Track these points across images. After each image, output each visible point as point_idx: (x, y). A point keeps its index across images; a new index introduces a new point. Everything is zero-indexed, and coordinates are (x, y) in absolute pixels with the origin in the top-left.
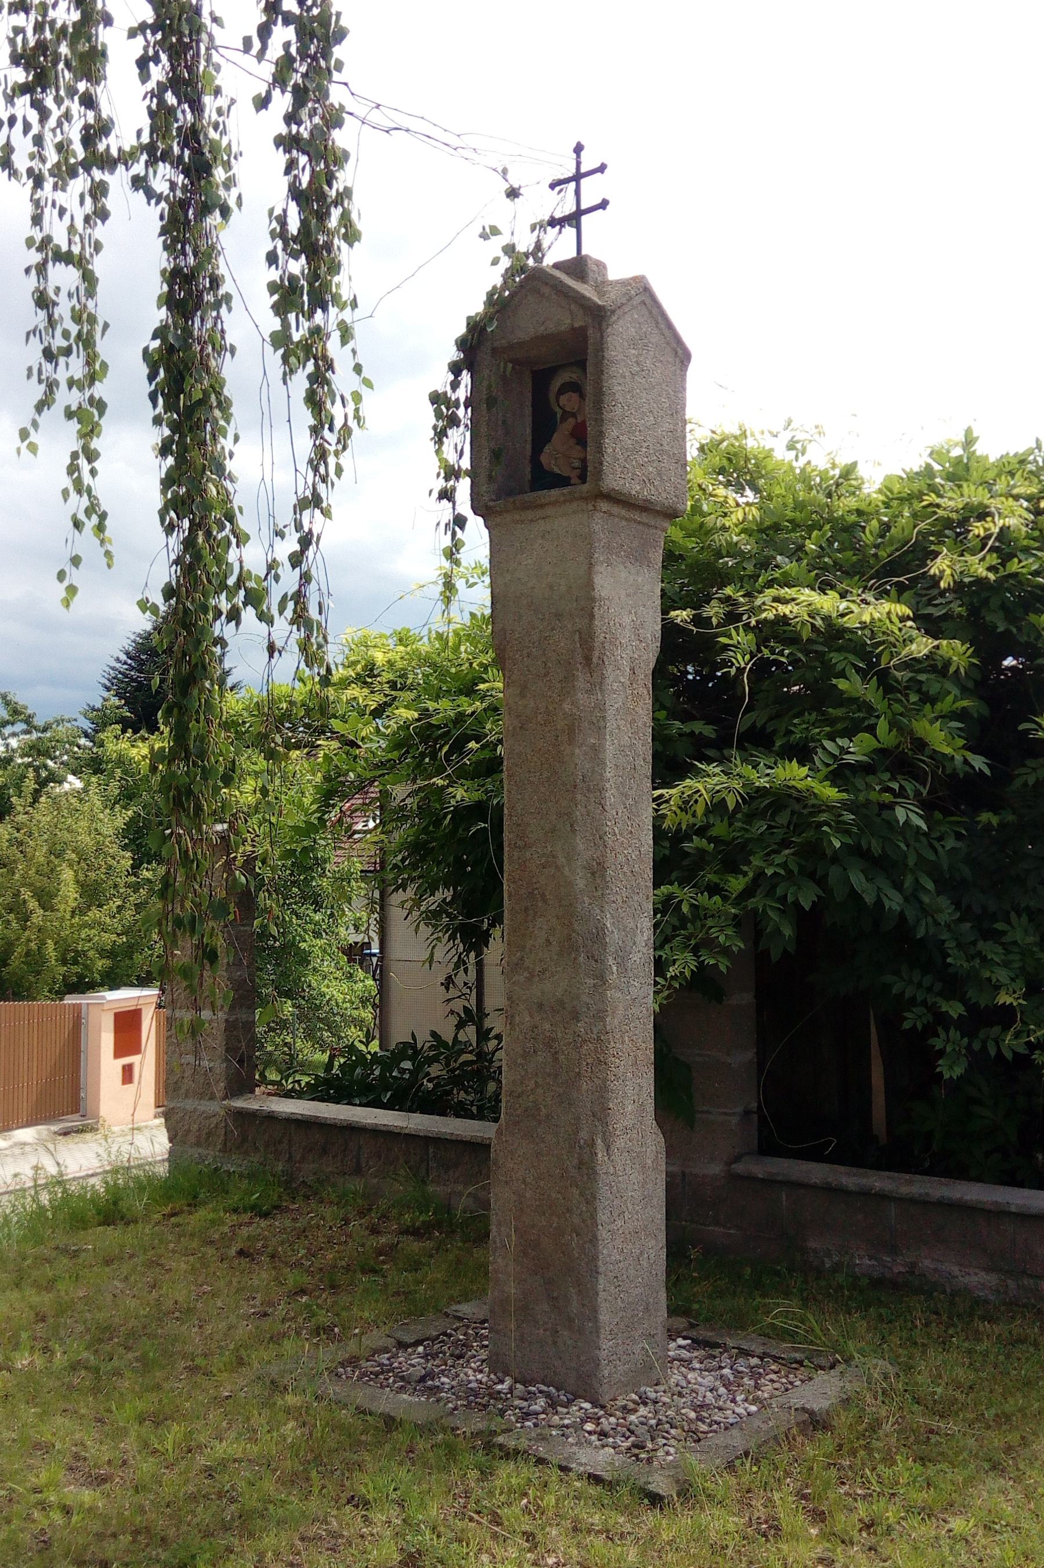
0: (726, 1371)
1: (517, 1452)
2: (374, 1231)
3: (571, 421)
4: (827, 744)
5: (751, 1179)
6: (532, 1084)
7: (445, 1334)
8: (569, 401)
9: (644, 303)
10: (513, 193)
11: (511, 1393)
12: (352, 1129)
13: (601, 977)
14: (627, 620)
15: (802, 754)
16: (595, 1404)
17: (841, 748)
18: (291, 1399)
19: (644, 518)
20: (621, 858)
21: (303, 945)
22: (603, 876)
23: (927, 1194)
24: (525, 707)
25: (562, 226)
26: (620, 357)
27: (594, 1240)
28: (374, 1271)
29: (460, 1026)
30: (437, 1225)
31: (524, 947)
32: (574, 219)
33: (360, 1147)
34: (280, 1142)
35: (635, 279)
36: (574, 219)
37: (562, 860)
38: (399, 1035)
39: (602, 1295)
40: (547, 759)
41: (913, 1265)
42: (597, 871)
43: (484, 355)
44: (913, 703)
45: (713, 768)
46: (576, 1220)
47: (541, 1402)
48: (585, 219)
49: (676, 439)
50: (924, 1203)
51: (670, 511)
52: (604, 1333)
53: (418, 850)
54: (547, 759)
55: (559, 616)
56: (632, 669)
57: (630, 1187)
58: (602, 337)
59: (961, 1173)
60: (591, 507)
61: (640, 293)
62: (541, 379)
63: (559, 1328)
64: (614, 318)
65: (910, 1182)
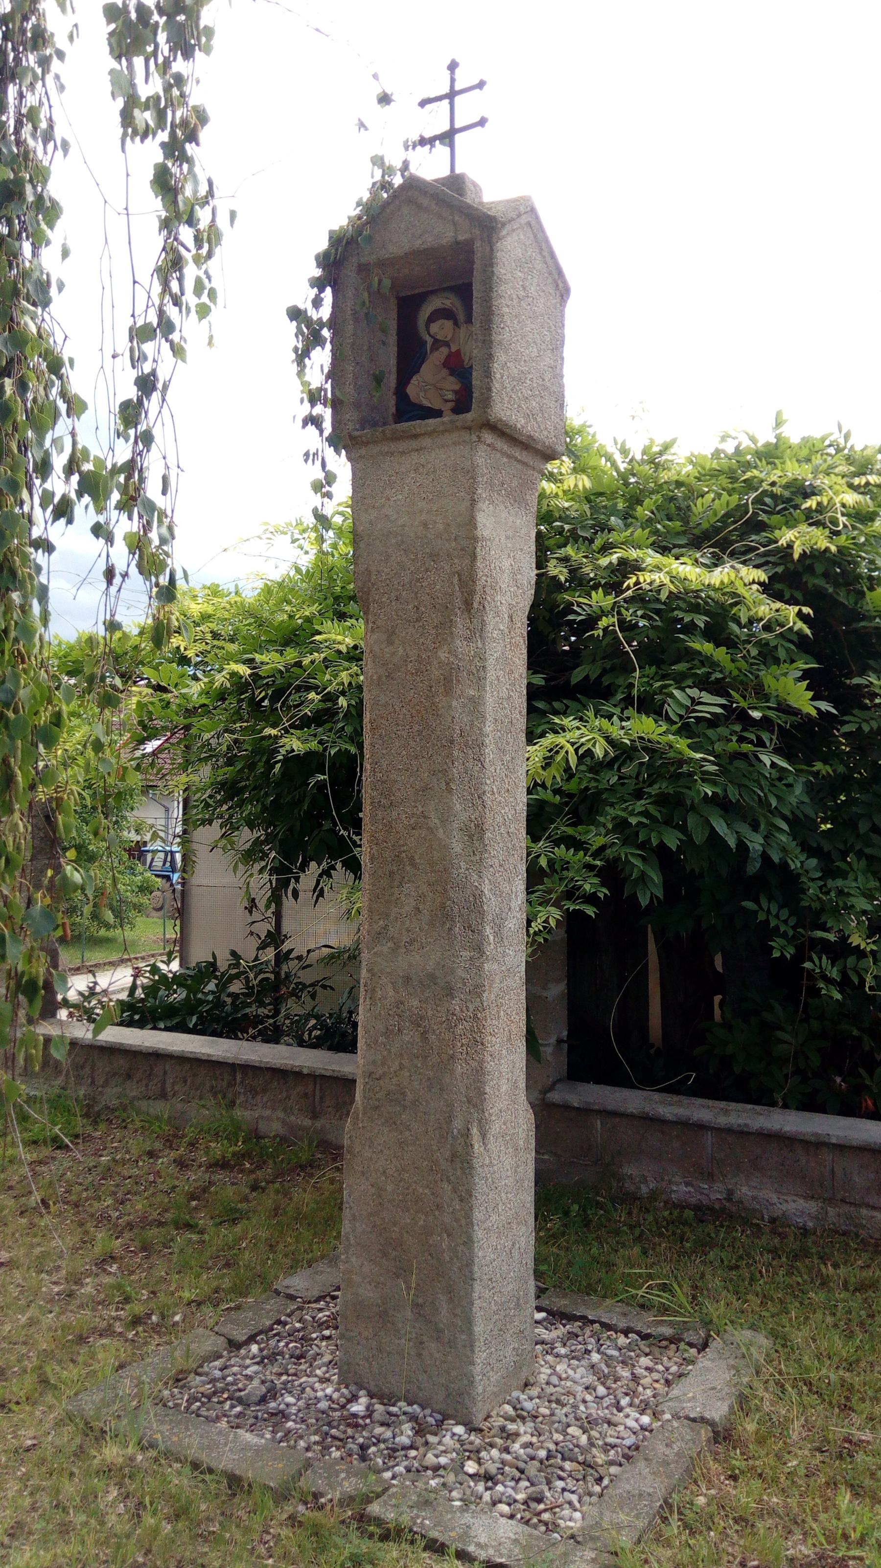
0: (595, 1357)
1: (399, 1531)
2: (182, 1164)
3: (444, 351)
4: (677, 693)
5: (567, 1107)
6: (395, 1066)
7: (279, 1322)
8: (441, 329)
9: (529, 224)
10: (385, 99)
11: (370, 1416)
12: (157, 1056)
13: (479, 949)
14: (506, 564)
15: (649, 705)
16: (472, 1429)
17: (693, 699)
18: (111, 1452)
19: (524, 456)
20: (499, 819)
21: (91, 847)
22: (481, 839)
23: (746, 1125)
24: (393, 654)
25: (433, 146)
26: (509, 276)
27: (469, 1242)
28: (189, 1226)
29: (263, 947)
30: (245, 1155)
31: (388, 915)
32: (448, 137)
33: (165, 1073)
34: (83, 1067)
35: (522, 198)
36: (448, 137)
37: (435, 821)
38: (199, 954)
39: (477, 1303)
40: (419, 712)
41: (730, 1193)
42: (475, 833)
43: (350, 273)
44: (754, 658)
45: (568, 721)
46: (447, 1219)
47: (407, 1429)
48: (458, 138)
49: (555, 377)
50: (743, 1133)
51: (549, 452)
52: (479, 1345)
53: (230, 790)
54: (419, 712)
55: (434, 556)
56: (511, 617)
57: (504, 1176)
58: (492, 250)
59: (762, 1097)
60: (474, 438)
61: (525, 213)
62: (408, 306)
63: (425, 1338)
64: (504, 232)
65: (726, 1112)
